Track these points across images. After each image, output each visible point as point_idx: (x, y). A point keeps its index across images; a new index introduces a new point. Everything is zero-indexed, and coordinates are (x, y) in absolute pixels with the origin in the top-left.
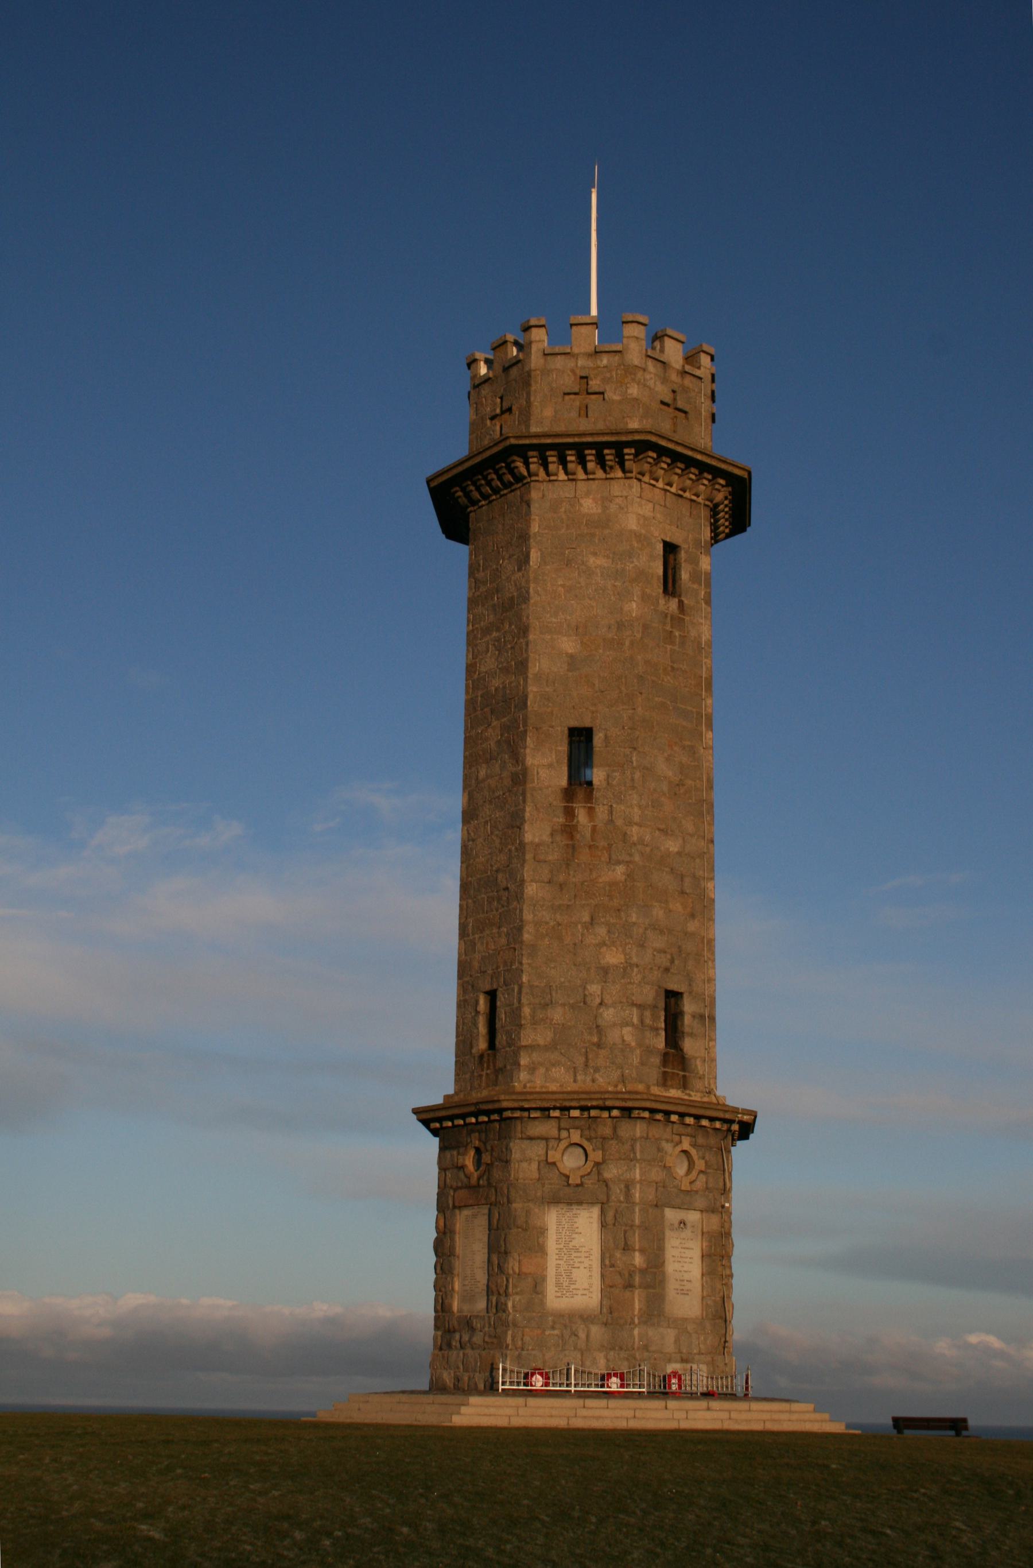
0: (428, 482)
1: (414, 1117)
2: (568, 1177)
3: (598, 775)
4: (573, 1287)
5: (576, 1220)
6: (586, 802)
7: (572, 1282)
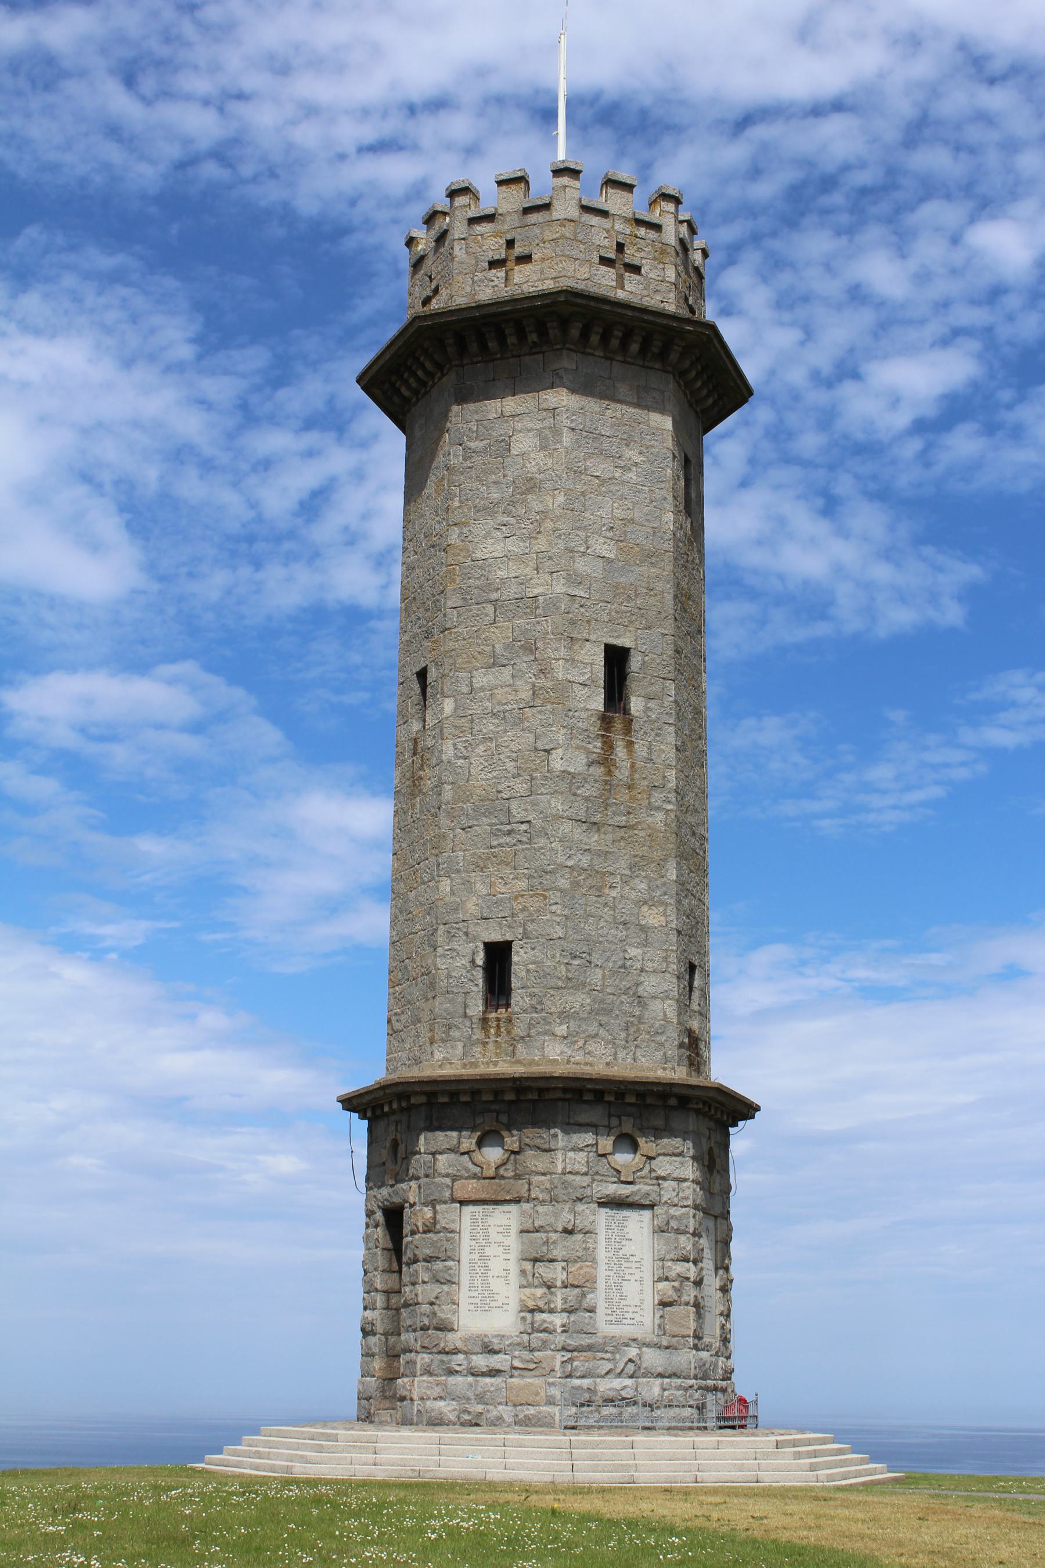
0: (358, 381)
1: (340, 1105)
2: (619, 1172)
3: (636, 705)
4: (623, 1302)
5: (626, 1223)
6: (626, 735)
7: (623, 1298)
